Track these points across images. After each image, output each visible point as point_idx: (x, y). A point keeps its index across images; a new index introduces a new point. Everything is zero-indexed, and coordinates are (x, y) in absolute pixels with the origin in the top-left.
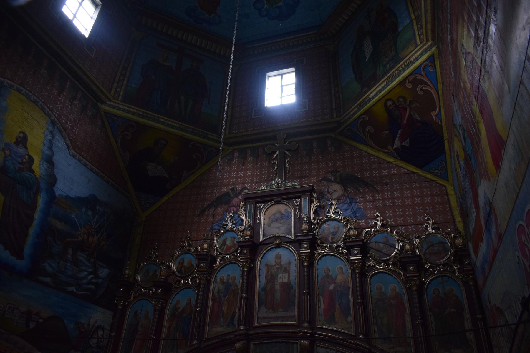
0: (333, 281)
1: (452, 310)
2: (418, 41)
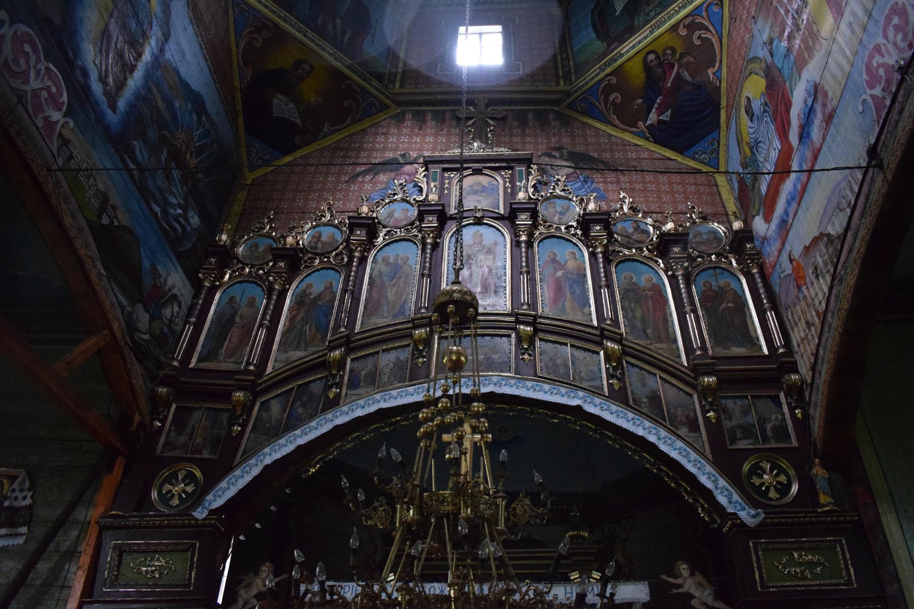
0: (562, 267)
1: (729, 305)
2: (573, 78)
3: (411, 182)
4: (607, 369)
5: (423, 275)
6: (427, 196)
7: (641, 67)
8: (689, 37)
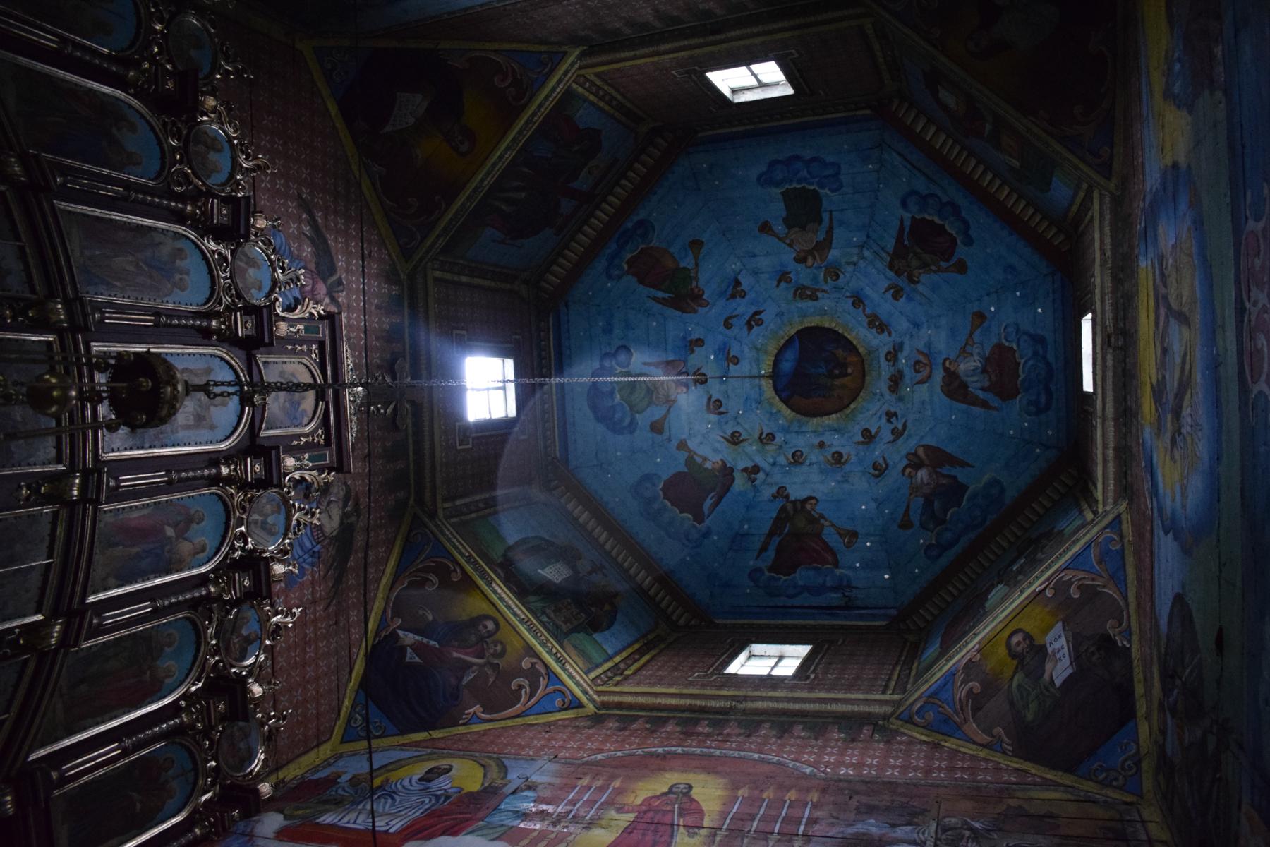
0: (181, 535)
1: (138, 806)
3: (301, 293)
4: (11, 630)
5: (157, 313)
6: (284, 319)
7: (475, 614)
8: (520, 673)
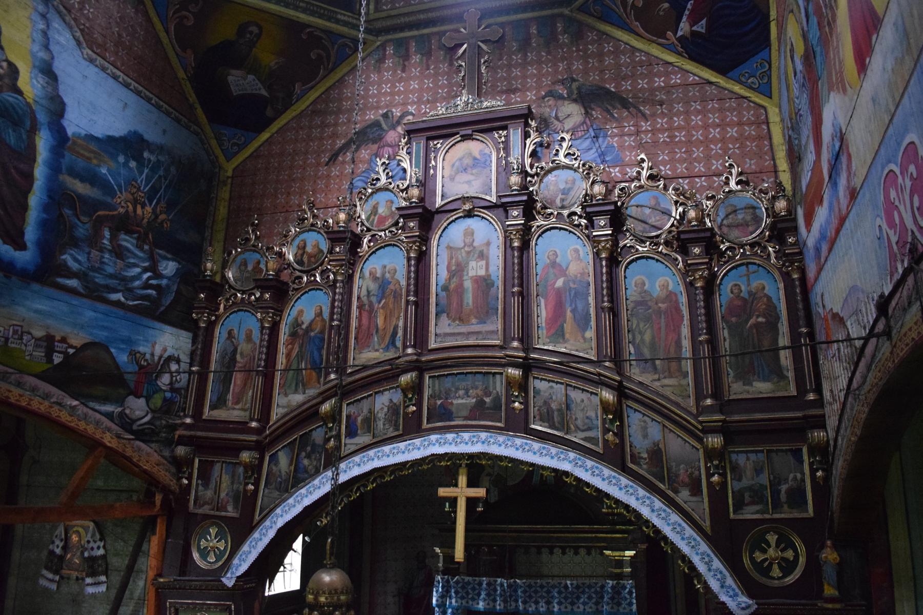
1: (760, 319)
